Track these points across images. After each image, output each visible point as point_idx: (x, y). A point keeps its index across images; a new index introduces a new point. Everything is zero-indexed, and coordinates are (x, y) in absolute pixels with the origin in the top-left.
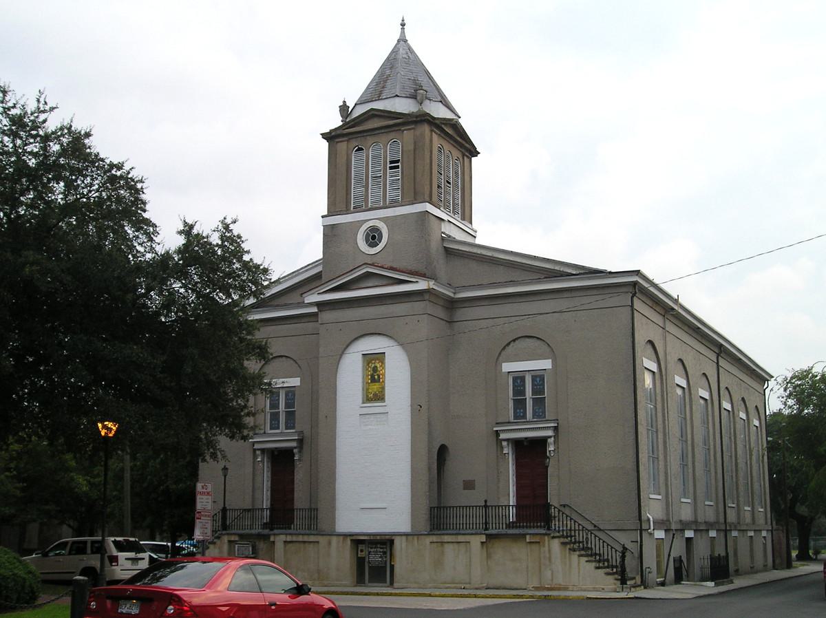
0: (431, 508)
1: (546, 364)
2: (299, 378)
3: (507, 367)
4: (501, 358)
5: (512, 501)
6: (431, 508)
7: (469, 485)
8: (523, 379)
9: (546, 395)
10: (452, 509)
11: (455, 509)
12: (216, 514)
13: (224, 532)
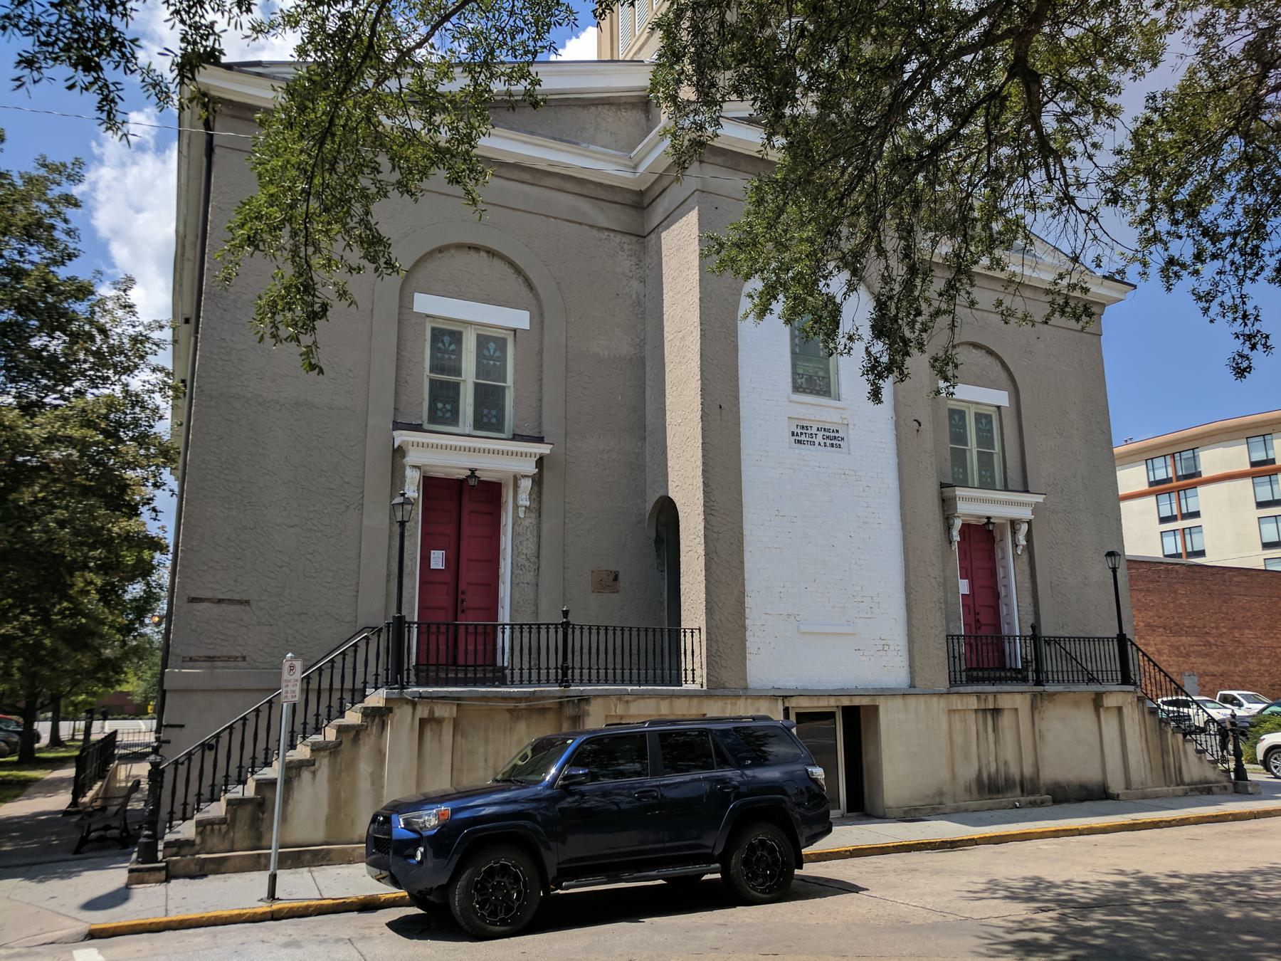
1: (520, 319)
3: (424, 303)
5: (416, 620)
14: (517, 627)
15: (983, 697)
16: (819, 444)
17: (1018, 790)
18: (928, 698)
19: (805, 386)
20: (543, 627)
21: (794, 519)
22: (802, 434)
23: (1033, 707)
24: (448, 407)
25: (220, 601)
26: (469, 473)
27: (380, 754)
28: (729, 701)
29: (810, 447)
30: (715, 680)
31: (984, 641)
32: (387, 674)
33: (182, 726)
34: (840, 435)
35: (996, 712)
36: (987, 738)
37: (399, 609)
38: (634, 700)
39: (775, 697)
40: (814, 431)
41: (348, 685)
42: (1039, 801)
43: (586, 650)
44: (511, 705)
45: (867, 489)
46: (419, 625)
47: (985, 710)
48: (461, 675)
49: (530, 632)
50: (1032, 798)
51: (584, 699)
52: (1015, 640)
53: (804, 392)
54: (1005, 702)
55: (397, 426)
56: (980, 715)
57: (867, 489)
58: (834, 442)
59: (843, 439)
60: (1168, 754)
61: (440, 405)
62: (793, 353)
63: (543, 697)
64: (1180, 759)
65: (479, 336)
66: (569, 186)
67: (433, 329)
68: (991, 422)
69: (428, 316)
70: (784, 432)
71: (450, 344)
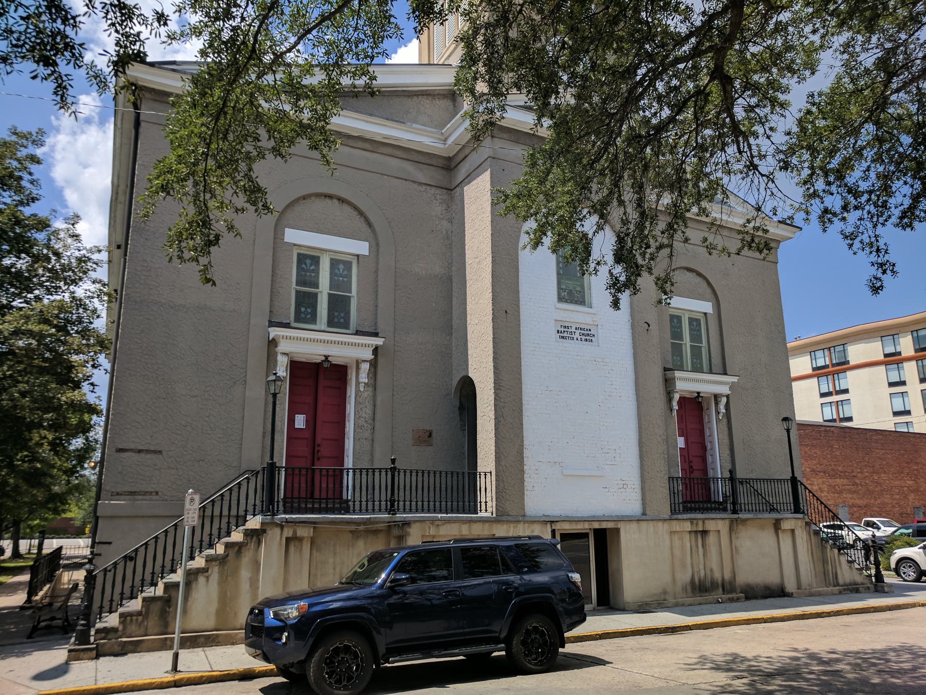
1: (362, 248)
3: (292, 236)
5: (284, 465)
14: (358, 471)
15: (695, 522)
19: (566, 298)
21: (559, 393)
23: (731, 530)
24: (342, 315)
25: (140, 451)
26: (323, 358)
27: (256, 564)
28: (512, 525)
30: (501, 509)
31: (696, 482)
32: (263, 505)
34: (592, 332)
35: (704, 533)
36: (698, 552)
37: (272, 457)
38: (443, 524)
39: (545, 522)
40: (573, 330)
42: (735, 598)
43: (408, 488)
45: (611, 372)
47: (696, 532)
48: (316, 506)
50: (730, 596)
53: (566, 302)
54: (711, 526)
55: (272, 324)
56: (693, 535)
57: (611, 372)
59: (594, 336)
61: (303, 309)
63: (376, 522)
64: (836, 568)
65: (332, 260)
66: (398, 153)
67: (299, 255)
68: (700, 324)
69: (295, 245)
70: (552, 329)
71: (311, 265)
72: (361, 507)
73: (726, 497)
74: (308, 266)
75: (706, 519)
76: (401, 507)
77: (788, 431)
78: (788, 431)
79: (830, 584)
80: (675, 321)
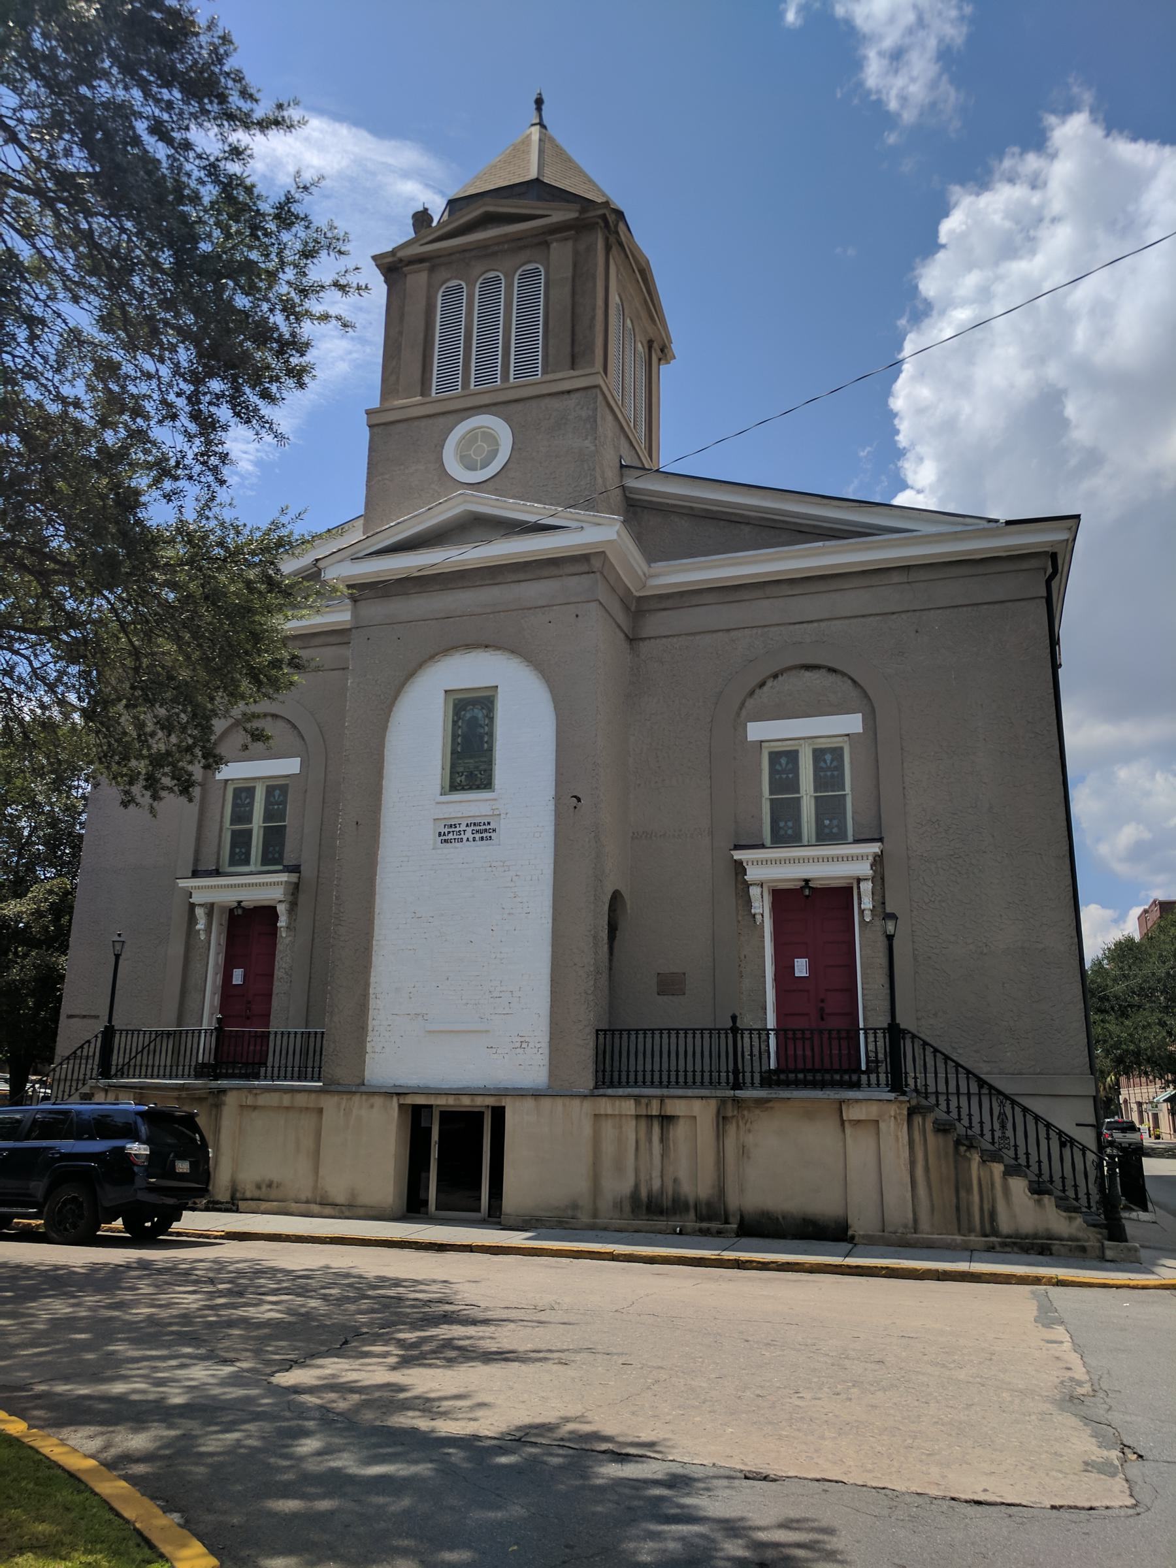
0: (597, 1031)
1: (853, 723)
2: (299, 759)
3: (756, 731)
4: (744, 713)
5: (771, 1023)
6: (597, 1031)
7: (670, 985)
8: (793, 756)
9: (848, 790)
10: (633, 1037)
11: (625, 1036)
12: (89, 1042)
13: (103, 1082)
14: (871, 1032)
15: (644, 1101)
16: (468, 840)
17: (692, 1215)
18: (567, 1100)
19: (464, 783)
20: (633, 1033)
21: (431, 920)
22: (449, 832)
23: (722, 1120)
24: (790, 824)
28: (345, 1097)
29: (457, 845)
33: (1077, 1125)
35: (666, 1120)
36: (650, 1149)
38: (262, 1093)
40: (463, 827)
41: (75, 1077)
42: (714, 1230)
43: (706, 1053)
44: (176, 1094)
45: (515, 878)
46: (777, 1031)
47: (650, 1117)
48: (237, 1071)
49: (677, 1037)
50: (705, 1225)
51: (223, 1091)
52: (768, 1035)
53: (463, 789)
54: (676, 1107)
55: (737, 847)
56: (643, 1123)
57: (515, 878)
58: (484, 835)
59: (494, 830)
60: (969, 1190)
61: (827, 822)
62: (454, 752)
64: (994, 1200)
65: (815, 751)
67: (771, 754)
68: (841, 757)
70: (428, 833)
71: (247, 798)
72: (694, 1079)
73: (877, 1061)
74: (828, 762)
75: (668, 1097)
76: (748, 1080)
77: (117, 957)
78: (117, 957)
79: (971, 1230)
80: (783, 761)
